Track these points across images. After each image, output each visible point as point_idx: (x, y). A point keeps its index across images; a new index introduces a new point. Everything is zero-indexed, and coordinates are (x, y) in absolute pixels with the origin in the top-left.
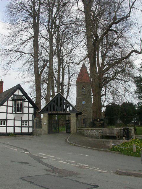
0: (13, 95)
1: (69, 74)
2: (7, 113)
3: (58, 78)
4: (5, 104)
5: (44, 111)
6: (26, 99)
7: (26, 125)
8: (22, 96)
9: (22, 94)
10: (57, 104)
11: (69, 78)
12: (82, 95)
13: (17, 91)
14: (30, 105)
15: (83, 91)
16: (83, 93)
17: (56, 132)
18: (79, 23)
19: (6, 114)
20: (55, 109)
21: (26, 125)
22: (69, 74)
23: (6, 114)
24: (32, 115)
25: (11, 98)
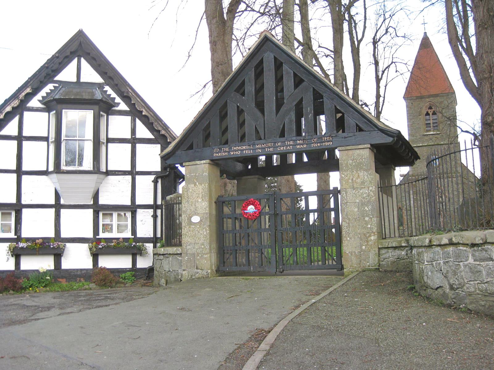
0: (50, 87)
1: (376, 63)
2: (19, 172)
3: (336, 70)
4: (11, 128)
5: (191, 147)
6: (118, 100)
7: (119, 231)
8: (100, 86)
9: (97, 79)
10: (260, 105)
11: (377, 76)
12: (426, 138)
13: (75, 61)
14: (143, 132)
15: (428, 125)
16: (430, 131)
17: (439, 230)
18: (432, 230)
19: (15, 175)
20: (249, 128)
21: (119, 231)
22: (376, 63)
23: (15, 175)
24: (155, 182)
25: (39, 96)
